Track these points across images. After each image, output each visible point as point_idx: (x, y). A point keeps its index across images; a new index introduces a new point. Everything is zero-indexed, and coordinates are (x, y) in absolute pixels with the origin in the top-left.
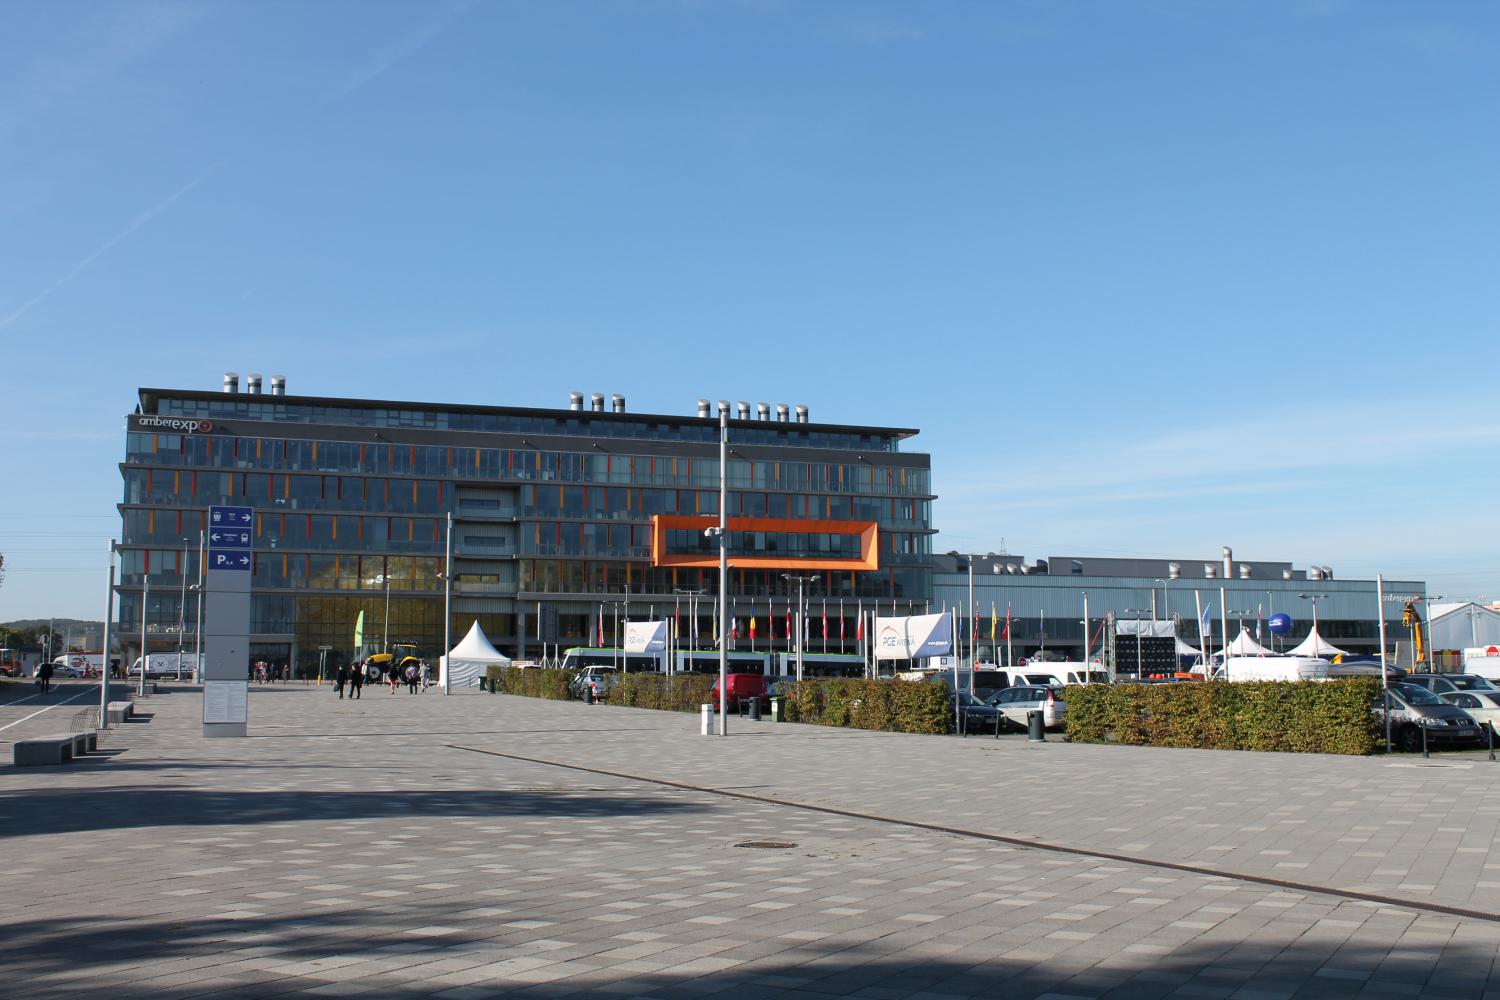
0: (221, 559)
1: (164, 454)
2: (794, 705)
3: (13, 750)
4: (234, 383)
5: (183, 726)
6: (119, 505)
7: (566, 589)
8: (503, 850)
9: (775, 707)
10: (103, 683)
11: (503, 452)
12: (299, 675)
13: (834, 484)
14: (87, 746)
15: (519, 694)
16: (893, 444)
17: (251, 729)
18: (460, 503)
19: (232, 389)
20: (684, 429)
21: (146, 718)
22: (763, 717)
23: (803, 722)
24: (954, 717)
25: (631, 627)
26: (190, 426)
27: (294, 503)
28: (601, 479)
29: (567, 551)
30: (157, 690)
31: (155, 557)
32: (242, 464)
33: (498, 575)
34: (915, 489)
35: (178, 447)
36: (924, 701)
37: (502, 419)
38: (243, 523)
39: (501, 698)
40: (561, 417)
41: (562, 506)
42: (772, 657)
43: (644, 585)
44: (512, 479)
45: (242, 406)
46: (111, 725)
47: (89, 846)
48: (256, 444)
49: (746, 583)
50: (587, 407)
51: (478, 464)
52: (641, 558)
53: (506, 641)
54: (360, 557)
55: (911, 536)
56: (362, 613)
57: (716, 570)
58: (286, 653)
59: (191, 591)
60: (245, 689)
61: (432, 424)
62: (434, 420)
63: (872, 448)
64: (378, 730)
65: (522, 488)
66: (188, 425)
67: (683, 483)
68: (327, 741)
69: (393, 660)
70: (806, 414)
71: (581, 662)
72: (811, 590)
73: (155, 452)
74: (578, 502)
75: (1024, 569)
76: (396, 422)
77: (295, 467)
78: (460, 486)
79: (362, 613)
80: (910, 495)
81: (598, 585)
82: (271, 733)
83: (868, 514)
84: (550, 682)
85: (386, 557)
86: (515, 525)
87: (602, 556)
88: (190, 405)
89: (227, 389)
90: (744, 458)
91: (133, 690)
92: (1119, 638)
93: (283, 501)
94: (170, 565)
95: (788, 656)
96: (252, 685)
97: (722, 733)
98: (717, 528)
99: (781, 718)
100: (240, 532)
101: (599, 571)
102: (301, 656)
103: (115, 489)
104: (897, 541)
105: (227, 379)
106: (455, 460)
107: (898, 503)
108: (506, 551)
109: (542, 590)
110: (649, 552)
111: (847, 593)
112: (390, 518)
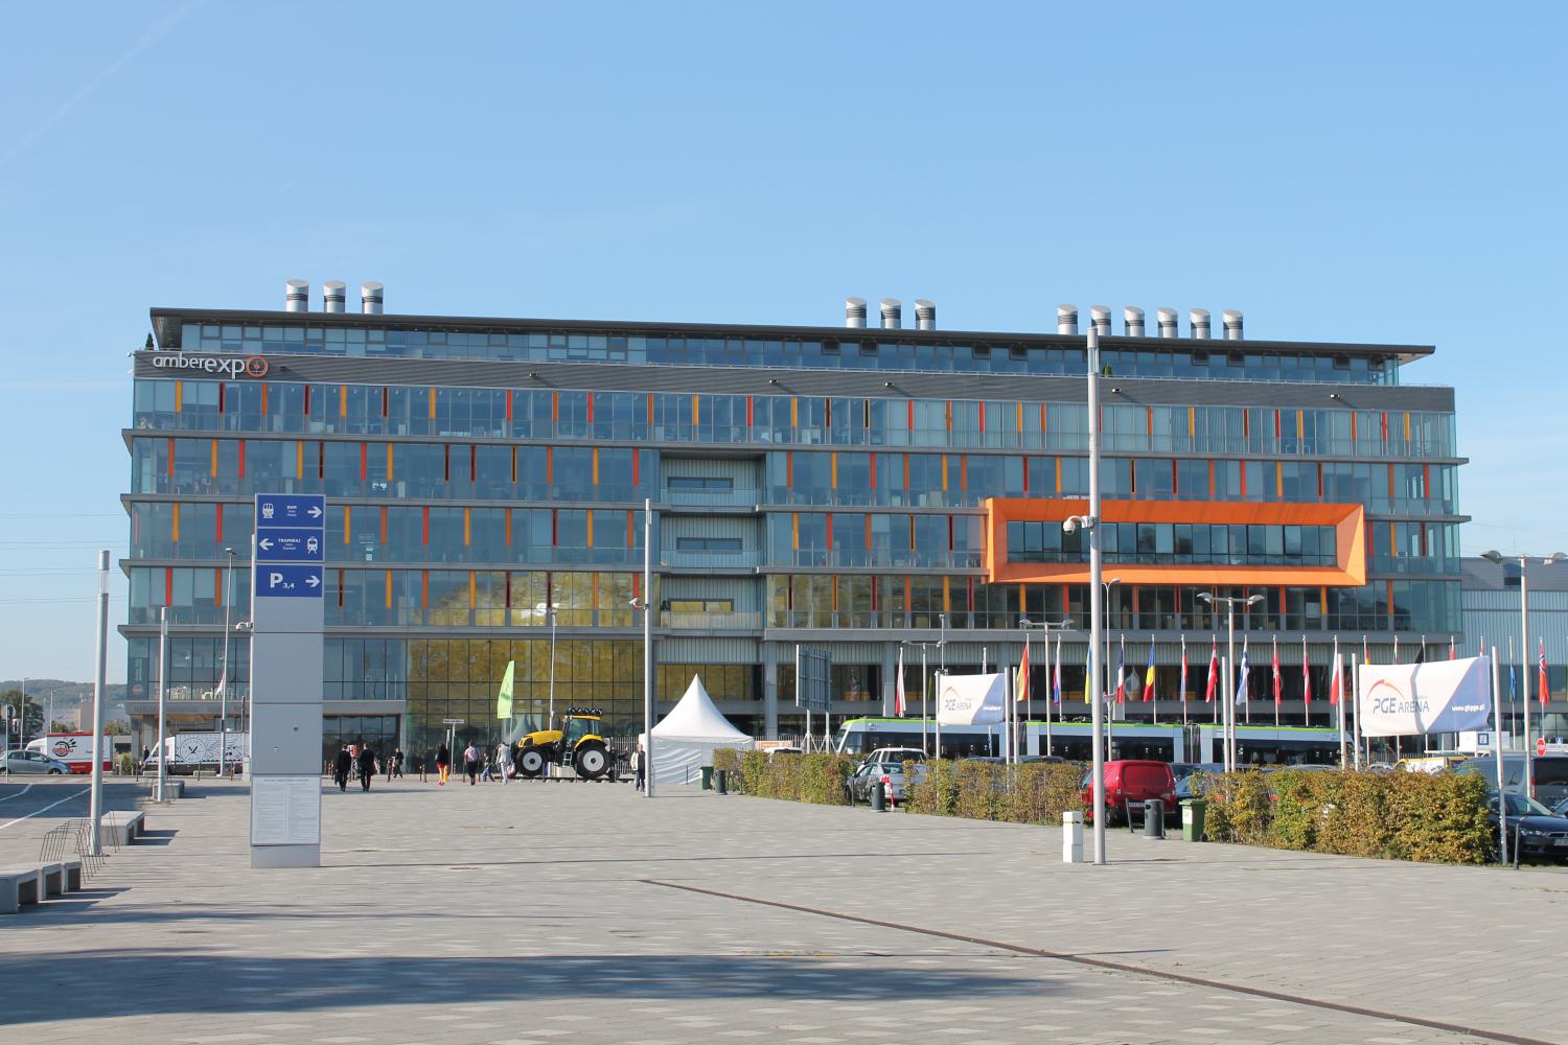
0: (275, 579)
2: (1221, 813)
4: (302, 297)
7: (843, 624)
12: (415, 766)
13: (1289, 444)
15: (765, 795)
16: (1390, 371)
18: (669, 485)
19: (299, 306)
21: (163, 837)
23: (1235, 841)
24: (1496, 834)
27: (402, 488)
28: (898, 440)
30: (184, 793)
31: (181, 578)
34: (1428, 446)
36: (1443, 807)
38: (272, 536)
39: (735, 802)
40: (830, 339)
41: (834, 485)
42: (1186, 733)
43: (971, 615)
44: (751, 443)
46: (105, 849)
50: (873, 322)
60: (318, 790)
61: (620, 355)
62: (625, 350)
64: (531, 855)
65: (769, 455)
66: (230, 365)
67: (1034, 445)
69: (564, 741)
70: (1239, 325)
73: (179, 409)
74: (861, 479)
76: (562, 354)
77: (402, 430)
78: (667, 456)
81: (895, 616)
83: (1349, 491)
84: (815, 774)
85: (549, 574)
86: (759, 517)
87: (901, 566)
88: (232, 332)
89: (291, 307)
91: (148, 792)
93: (384, 486)
97: (1097, 859)
98: (1085, 518)
99: (1199, 835)
100: (304, 536)
103: (117, 469)
104: (1398, 536)
105: (291, 290)
107: (1399, 471)
108: (744, 560)
110: (978, 560)
112: (555, 510)
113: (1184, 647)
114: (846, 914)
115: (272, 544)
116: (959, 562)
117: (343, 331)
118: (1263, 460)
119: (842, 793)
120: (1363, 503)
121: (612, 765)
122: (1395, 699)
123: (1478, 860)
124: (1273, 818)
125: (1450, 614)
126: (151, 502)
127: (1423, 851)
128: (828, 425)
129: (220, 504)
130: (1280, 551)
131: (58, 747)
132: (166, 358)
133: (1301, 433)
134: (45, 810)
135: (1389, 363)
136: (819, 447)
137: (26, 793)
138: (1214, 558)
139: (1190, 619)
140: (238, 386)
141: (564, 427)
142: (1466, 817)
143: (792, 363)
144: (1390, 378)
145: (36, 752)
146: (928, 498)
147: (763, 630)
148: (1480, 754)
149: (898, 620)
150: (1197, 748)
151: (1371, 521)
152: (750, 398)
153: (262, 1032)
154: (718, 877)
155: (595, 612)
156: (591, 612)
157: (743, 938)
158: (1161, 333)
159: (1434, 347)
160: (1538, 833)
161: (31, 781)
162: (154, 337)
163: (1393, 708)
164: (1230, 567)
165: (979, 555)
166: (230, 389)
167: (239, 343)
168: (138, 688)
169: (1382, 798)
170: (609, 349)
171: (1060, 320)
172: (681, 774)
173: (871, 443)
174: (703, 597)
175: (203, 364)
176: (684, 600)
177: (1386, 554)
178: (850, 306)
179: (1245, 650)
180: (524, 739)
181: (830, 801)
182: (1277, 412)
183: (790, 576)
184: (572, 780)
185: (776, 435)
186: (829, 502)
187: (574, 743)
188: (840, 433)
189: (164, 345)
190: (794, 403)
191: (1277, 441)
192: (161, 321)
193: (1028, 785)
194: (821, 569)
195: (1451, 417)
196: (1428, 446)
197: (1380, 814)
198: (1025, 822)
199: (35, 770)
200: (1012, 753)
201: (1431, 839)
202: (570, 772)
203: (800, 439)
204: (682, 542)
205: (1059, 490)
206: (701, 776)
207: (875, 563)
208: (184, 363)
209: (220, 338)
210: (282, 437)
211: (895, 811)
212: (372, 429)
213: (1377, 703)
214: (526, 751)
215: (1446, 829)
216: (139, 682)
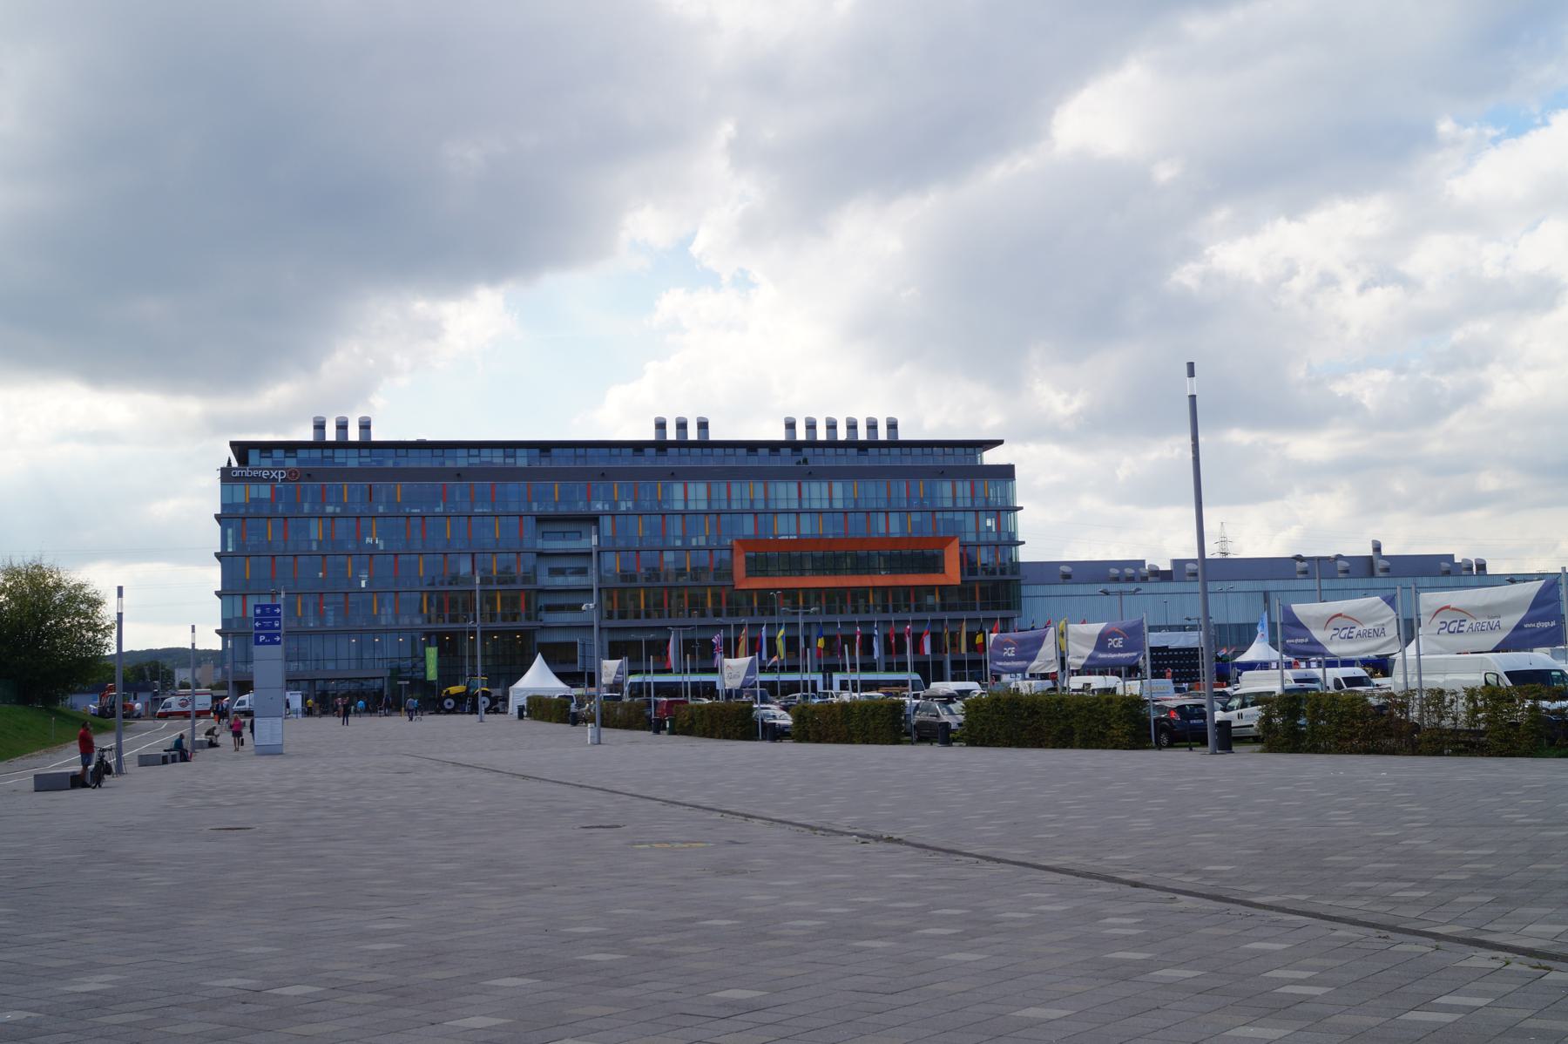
0: (262, 638)
10: (764, 633)
28: (679, 506)
38: (260, 621)
40: (638, 447)
45: (328, 452)
48: (343, 488)
62: (514, 456)
65: (601, 517)
66: (277, 474)
73: (248, 501)
92: (1152, 649)
100: (273, 620)
140: (281, 486)
180: (445, 691)
208: (250, 473)
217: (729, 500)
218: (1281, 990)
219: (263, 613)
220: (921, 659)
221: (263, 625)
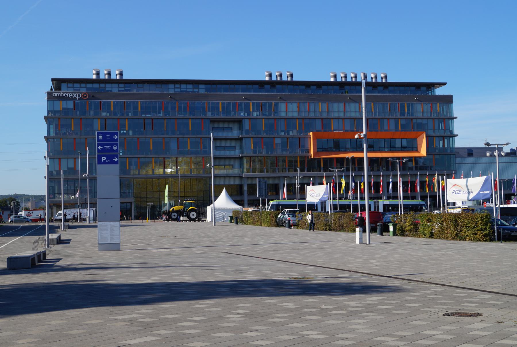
0: (103, 159)
1: (65, 110)
2: (401, 227)
3: (6, 260)
4: (98, 74)
5: (87, 245)
6: (45, 137)
7: (267, 171)
8: (306, 320)
9: (391, 228)
11: (233, 103)
12: (137, 218)
13: (402, 113)
14: (42, 257)
15: (250, 224)
16: (433, 91)
17: (122, 246)
18: (213, 130)
19: (97, 77)
20: (324, 87)
21: (67, 242)
22: (384, 234)
23: (406, 236)
24: (494, 232)
25: (309, 189)
26: (76, 95)
27: (131, 133)
28: (283, 115)
29: (267, 152)
30: (70, 228)
31: (64, 161)
32: (104, 114)
33: (233, 165)
34: (445, 113)
35: (72, 107)
36: (476, 224)
37: (232, 86)
38: (102, 145)
39: (241, 227)
40: (261, 84)
41: (264, 129)
42: (375, 203)
43: (306, 168)
44: (238, 117)
45: (102, 85)
46: (51, 246)
47: (61, 322)
48: (110, 103)
49: (358, 165)
50: (274, 78)
51: (221, 110)
52: (305, 154)
53: (238, 198)
54: (164, 158)
55: (444, 138)
56: (167, 186)
57: (363, 158)
58: (130, 207)
59: (84, 178)
60: (119, 226)
61: (196, 90)
62: (198, 88)
63: (421, 93)
64: (186, 245)
65: (243, 120)
67: (325, 115)
68: (162, 252)
69: (184, 209)
70: (386, 77)
71: (278, 208)
72: (404, 167)
73: (61, 109)
74: (271, 127)
75: (503, 154)
76: (179, 90)
77: (130, 114)
78: (212, 121)
79: (167, 186)
80: (442, 117)
81: (283, 169)
82: (132, 248)
83: (421, 128)
84: (267, 218)
85: (177, 158)
86: (240, 140)
87: (285, 153)
88: (77, 85)
89: (94, 77)
90: (355, 101)
91: (58, 227)
93: (125, 132)
94: (71, 165)
95: (383, 202)
96: (122, 224)
97: (368, 243)
98: (362, 134)
99: (395, 234)
100: (112, 145)
101: (284, 161)
102: (137, 207)
103: (43, 129)
104: (436, 140)
105: (94, 72)
106: (209, 108)
107: (436, 122)
108: (236, 153)
109: (255, 172)
110: (308, 151)
111: (411, 169)
112: (178, 138)
113: (372, 177)
114: (301, 263)
115: (102, 148)
116: (302, 151)
117: (111, 84)
118: (394, 119)
119: (275, 223)
120: (425, 131)
121: (199, 216)
122: (461, 190)
123: (488, 240)
124: (419, 228)
125: (452, 165)
126: (54, 138)
127: (470, 238)
128: (261, 110)
129: (74, 138)
130: (400, 146)
131: (28, 214)
132: (57, 94)
133: (406, 110)
134: (27, 234)
135: (432, 88)
136: (259, 117)
137: (20, 229)
138: (380, 149)
139: (373, 168)
140: (79, 102)
141: (180, 113)
142: (484, 226)
143: (250, 92)
144: (433, 93)
145: (21, 216)
146: (292, 132)
147: (242, 174)
148: (463, 207)
149: (284, 170)
150: (378, 207)
151: (428, 137)
152: (237, 102)
153: (139, 314)
154: (249, 251)
155: (191, 170)
156: (190, 169)
157: (276, 272)
158: (352, 80)
159: (446, 83)
160: (506, 231)
161: (21, 225)
162: (53, 87)
163: (460, 193)
164: (385, 152)
165: (308, 149)
166: (77, 103)
167: (79, 88)
168: (51, 195)
169: (456, 221)
170: (193, 89)
171: (331, 77)
172: (222, 218)
173: (275, 116)
174: (224, 164)
175: (68, 95)
176: (218, 165)
177: (432, 147)
178: (267, 74)
179: (391, 177)
180: (172, 209)
181: (272, 226)
182: (399, 104)
183: (251, 157)
184: (187, 221)
185: (245, 114)
186: (262, 134)
187: (187, 210)
188: (265, 113)
189: (56, 90)
190: (251, 104)
191: (399, 113)
192: (54, 82)
193: (337, 220)
194: (260, 155)
195: (452, 104)
196: (445, 113)
197: (455, 226)
198: (336, 231)
199: (21, 221)
200: (331, 210)
201: (472, 234)
202: (186, 218)
203: (253, 115)
204: (217, 147)
205: (332, 129)
206: (229, 219)
207: (277, 153)
208: (62, 95)
209: (73, 87)
210: (93, 117)
211: (294, 229)
212: (121, 114)
213: (454, 191)
214: (172, 212)
215: (477, 230)
216: (51, 194)
217: (309, 111)
218: (471, 333)
219: (104, 139)
220: (433, 194)
221: (104, 148)
